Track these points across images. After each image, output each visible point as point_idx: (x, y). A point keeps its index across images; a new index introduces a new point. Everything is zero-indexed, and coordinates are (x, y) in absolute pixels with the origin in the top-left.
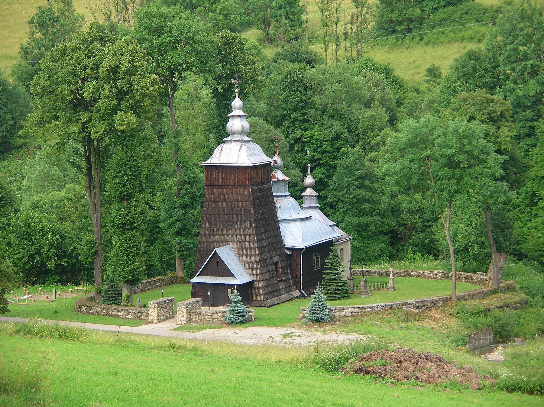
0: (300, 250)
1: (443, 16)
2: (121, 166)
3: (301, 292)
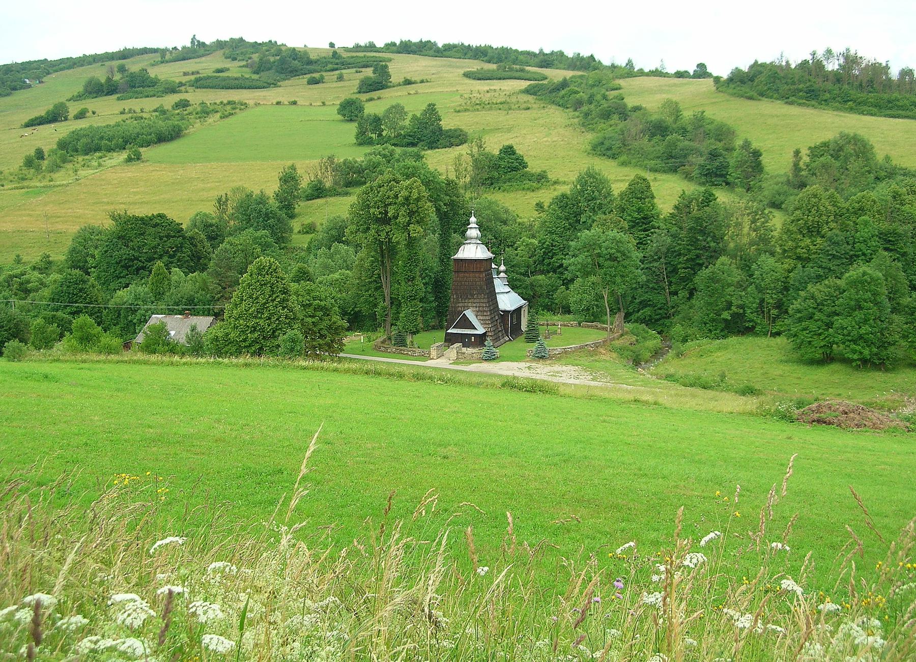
0: (509, 311)
1: (510, 177)
2: (409, 260)
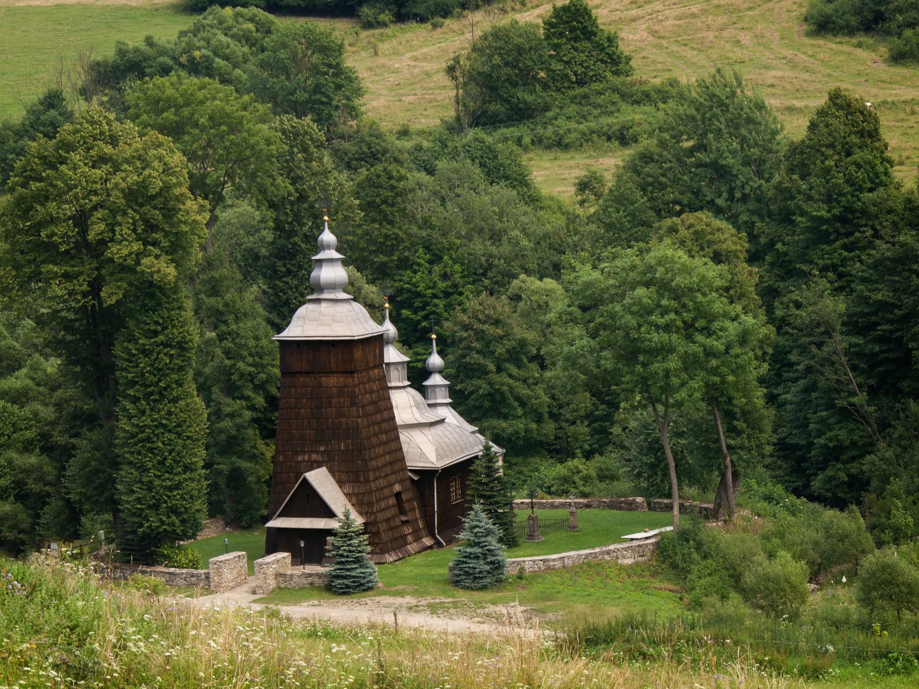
3: (436, 539)
